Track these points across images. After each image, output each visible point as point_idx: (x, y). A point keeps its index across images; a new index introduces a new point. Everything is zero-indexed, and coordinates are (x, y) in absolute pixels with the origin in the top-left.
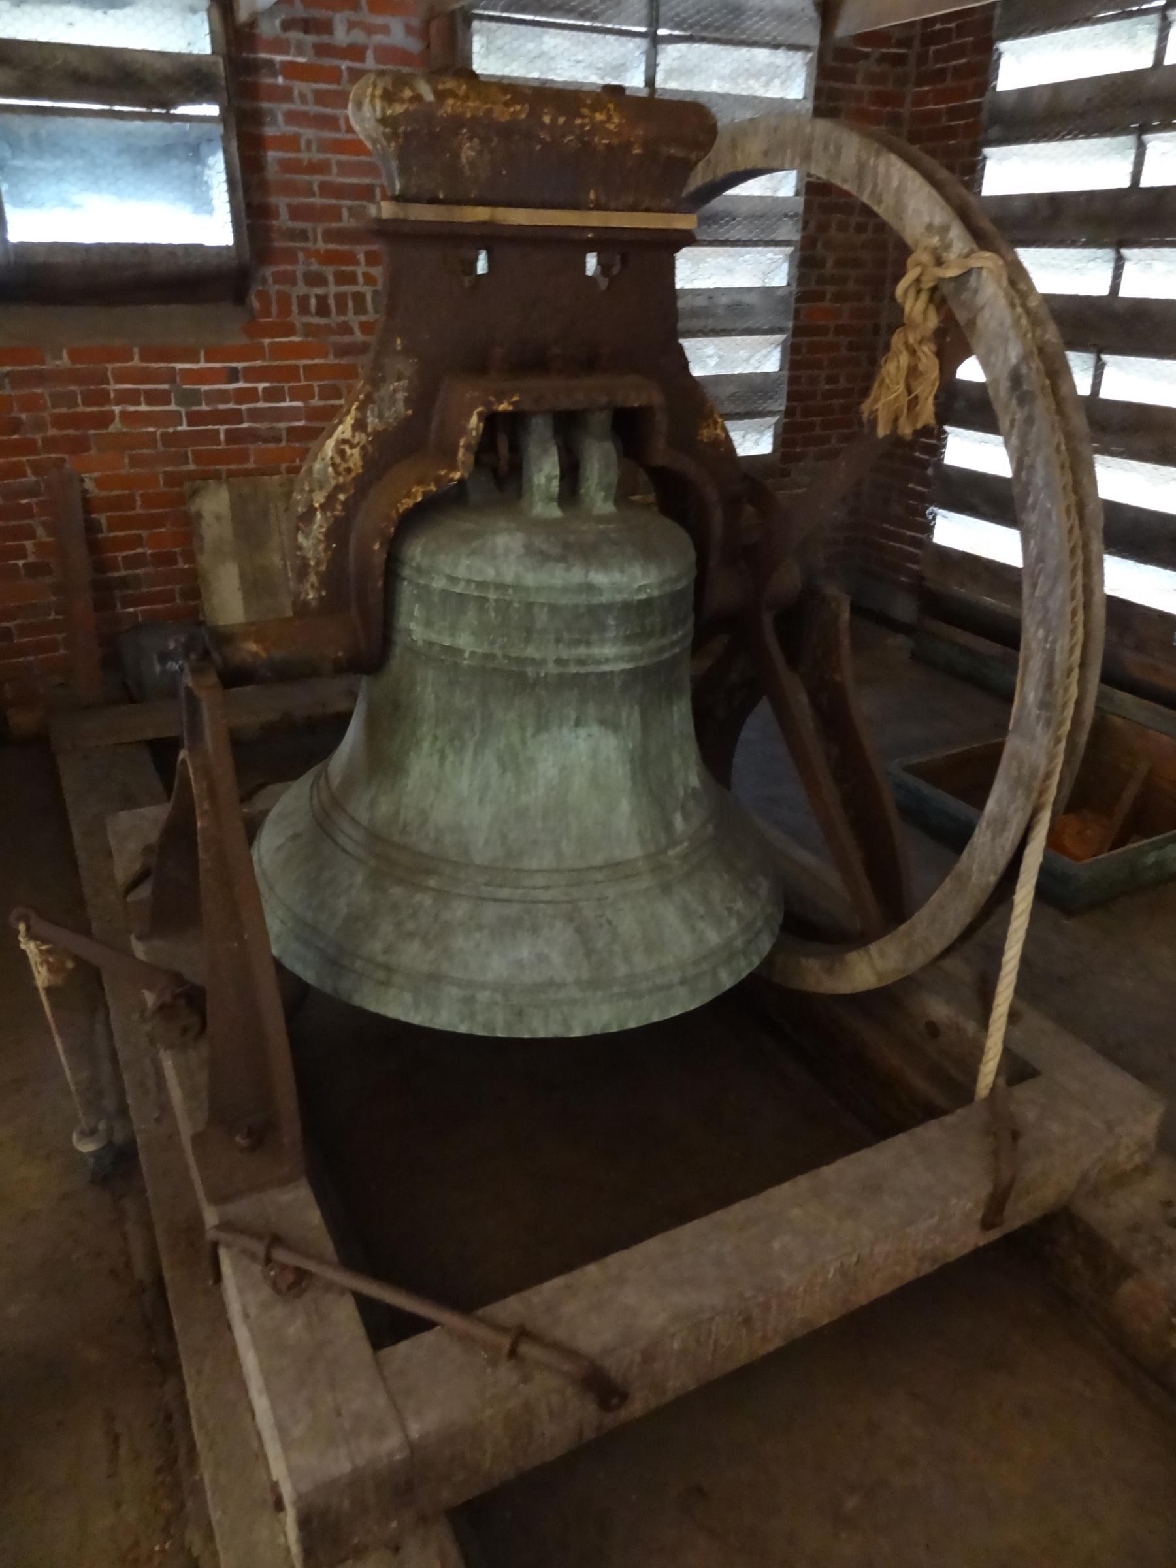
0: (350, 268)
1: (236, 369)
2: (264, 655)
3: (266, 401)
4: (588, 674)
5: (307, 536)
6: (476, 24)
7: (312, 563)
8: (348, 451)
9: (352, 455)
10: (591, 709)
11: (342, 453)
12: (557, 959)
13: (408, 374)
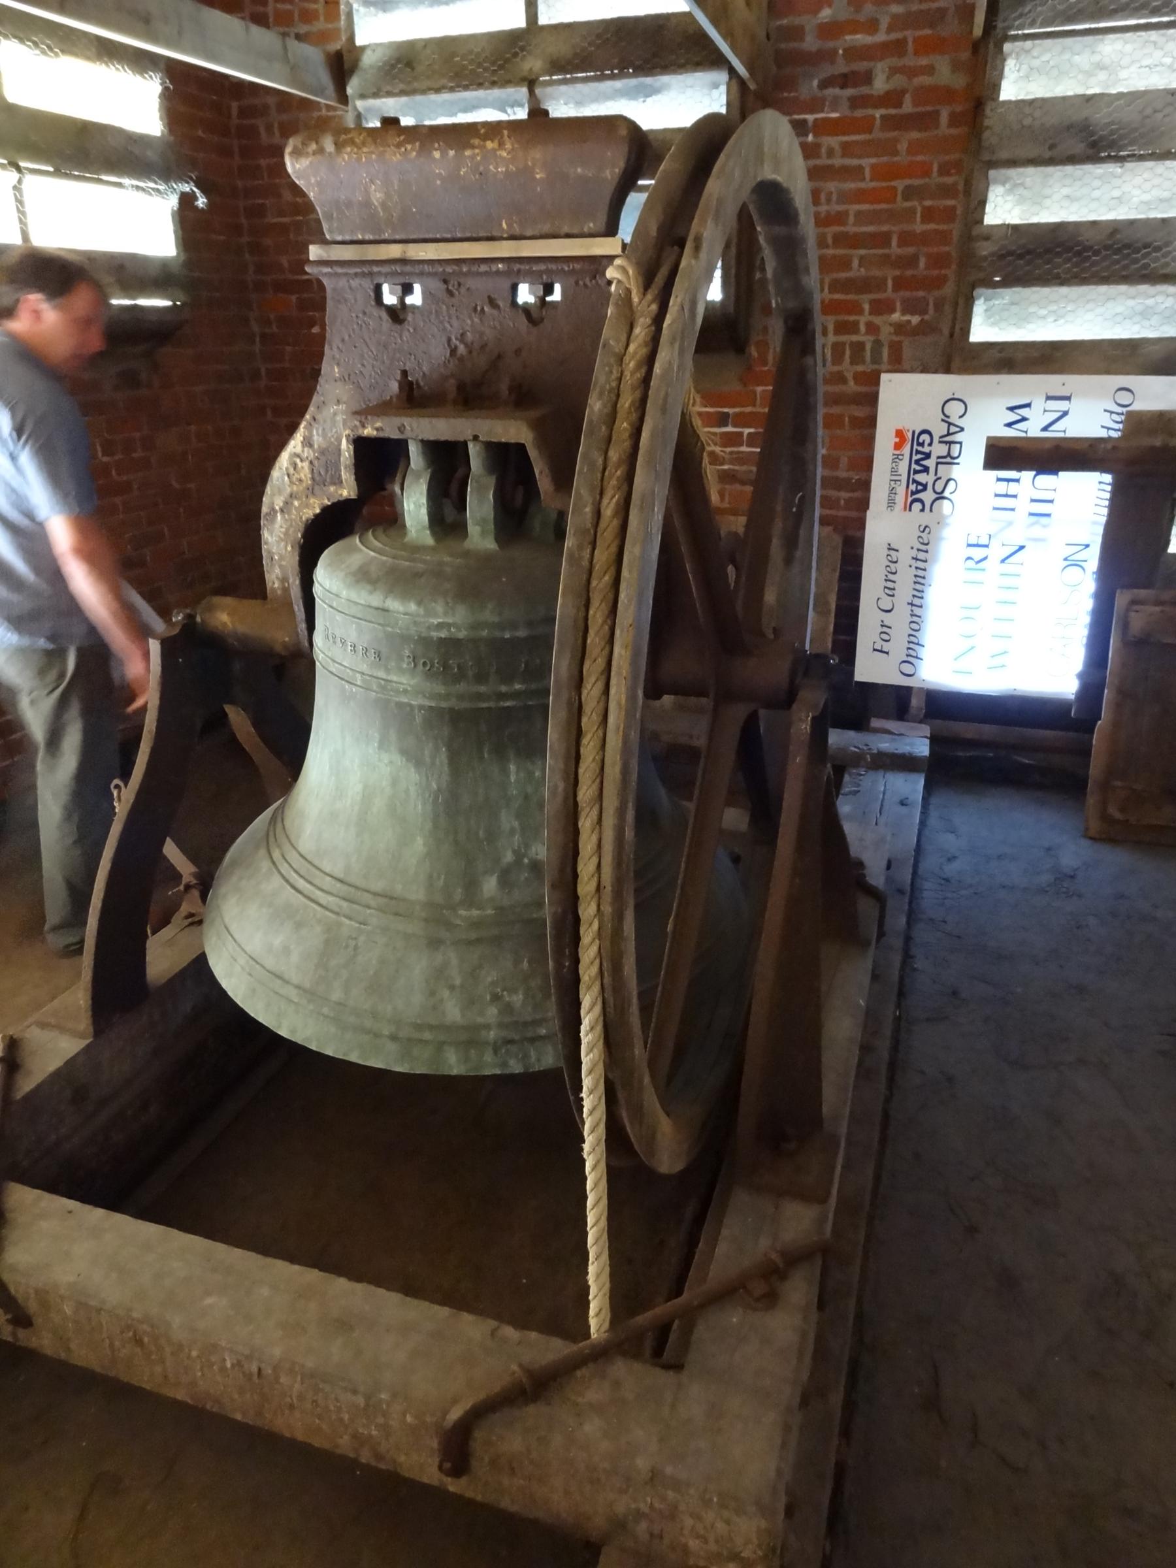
0: (852, 318)
1: (727, 414)
3: (749, 445)
6: (1007, 47)
8: (299, 464)
11: (295, 466)
12: (295, 958)
13: (345, 399)
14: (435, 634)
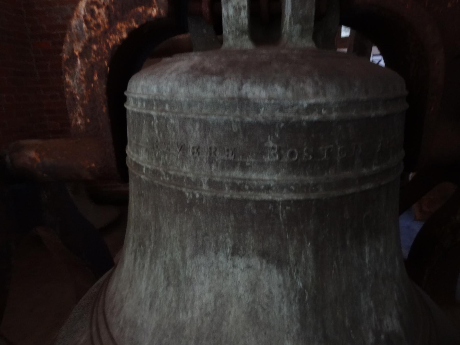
2: (39, 160)
4: (246, 201)
5: (72, 77)
7: (78, 98)
9: (99, 14)
10: (250, 239)
11: (92, 12)
14: (306, 118)
